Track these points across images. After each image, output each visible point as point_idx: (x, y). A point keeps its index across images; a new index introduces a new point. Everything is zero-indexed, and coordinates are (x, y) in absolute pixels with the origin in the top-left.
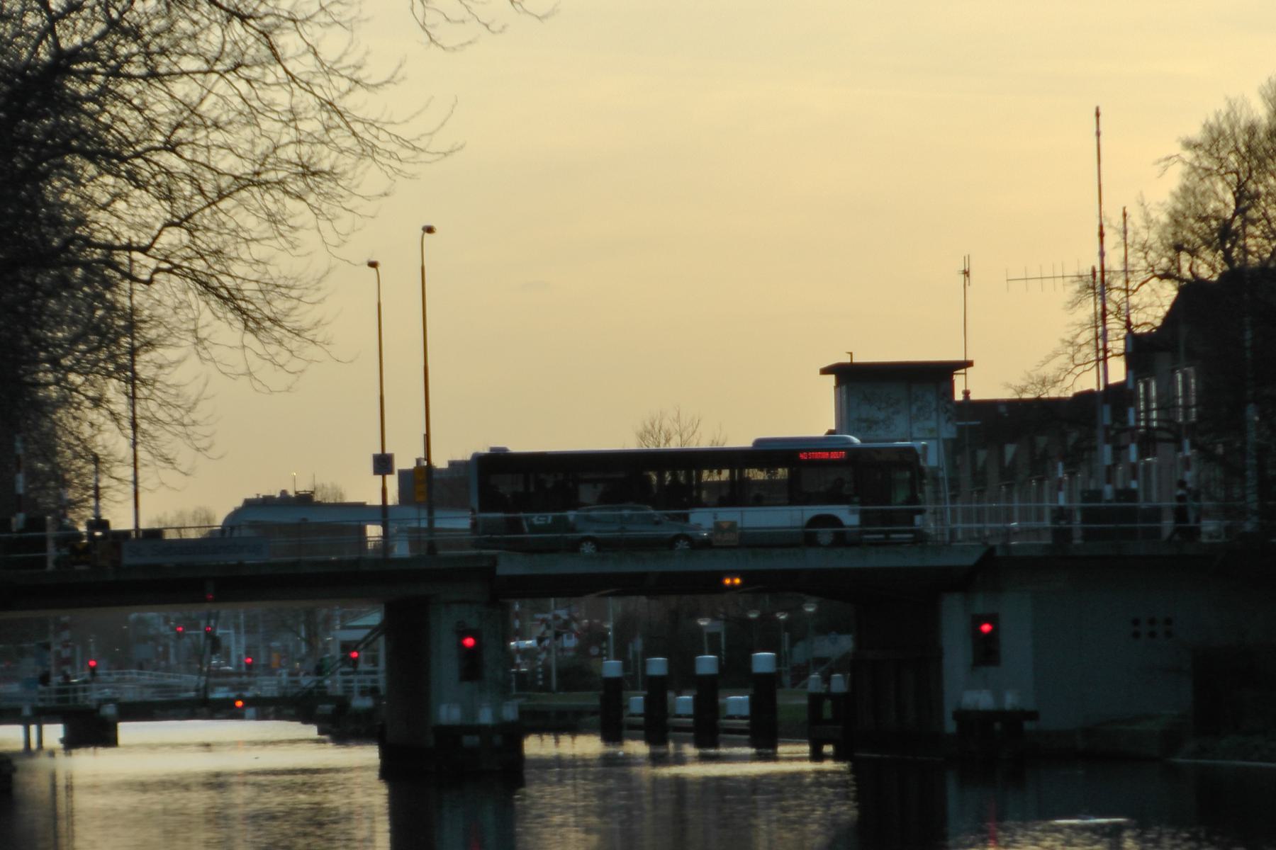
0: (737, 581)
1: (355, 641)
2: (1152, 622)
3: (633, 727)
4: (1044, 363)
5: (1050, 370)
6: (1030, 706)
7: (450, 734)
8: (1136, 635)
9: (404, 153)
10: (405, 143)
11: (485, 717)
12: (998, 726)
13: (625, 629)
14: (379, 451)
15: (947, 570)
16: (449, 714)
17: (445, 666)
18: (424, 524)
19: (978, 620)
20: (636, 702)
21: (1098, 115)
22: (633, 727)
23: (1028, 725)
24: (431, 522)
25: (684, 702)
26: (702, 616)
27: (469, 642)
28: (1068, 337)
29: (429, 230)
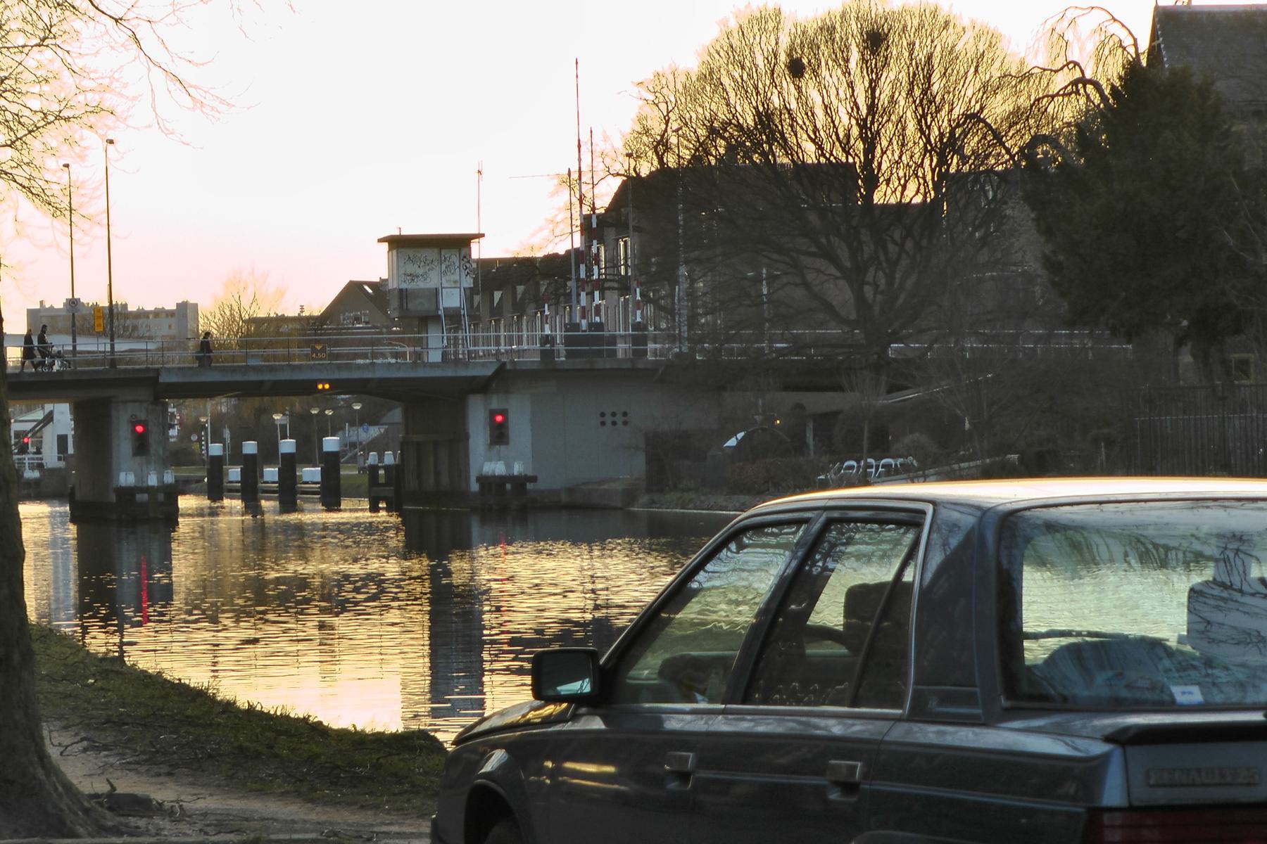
0: (327, 386)
1: (24, 431)
2: (614, 414)
3: (231, 490)
4: (534, 234)
5: (537, 240)
6: (530, 473)
7: (127, 494)
8: (603, 423)
9: (221, 107)
10: (222, 101)
11: (153, 481)
12: (508, 486)
13: (218, 421)
14: (71, 297)
15: (474, 378)
16: (126, 478)
17: (123, 445)
18: (108, 348)
19: (493, 413)
20: (234, 473)
21: (577, 63)
22: (231, 490)
23: (529, 486)
24: (112, 346)
25: (271, 473)
26: (277, 413)
27: (139, 429)
28: (549, 217)
29: (111, 142)
